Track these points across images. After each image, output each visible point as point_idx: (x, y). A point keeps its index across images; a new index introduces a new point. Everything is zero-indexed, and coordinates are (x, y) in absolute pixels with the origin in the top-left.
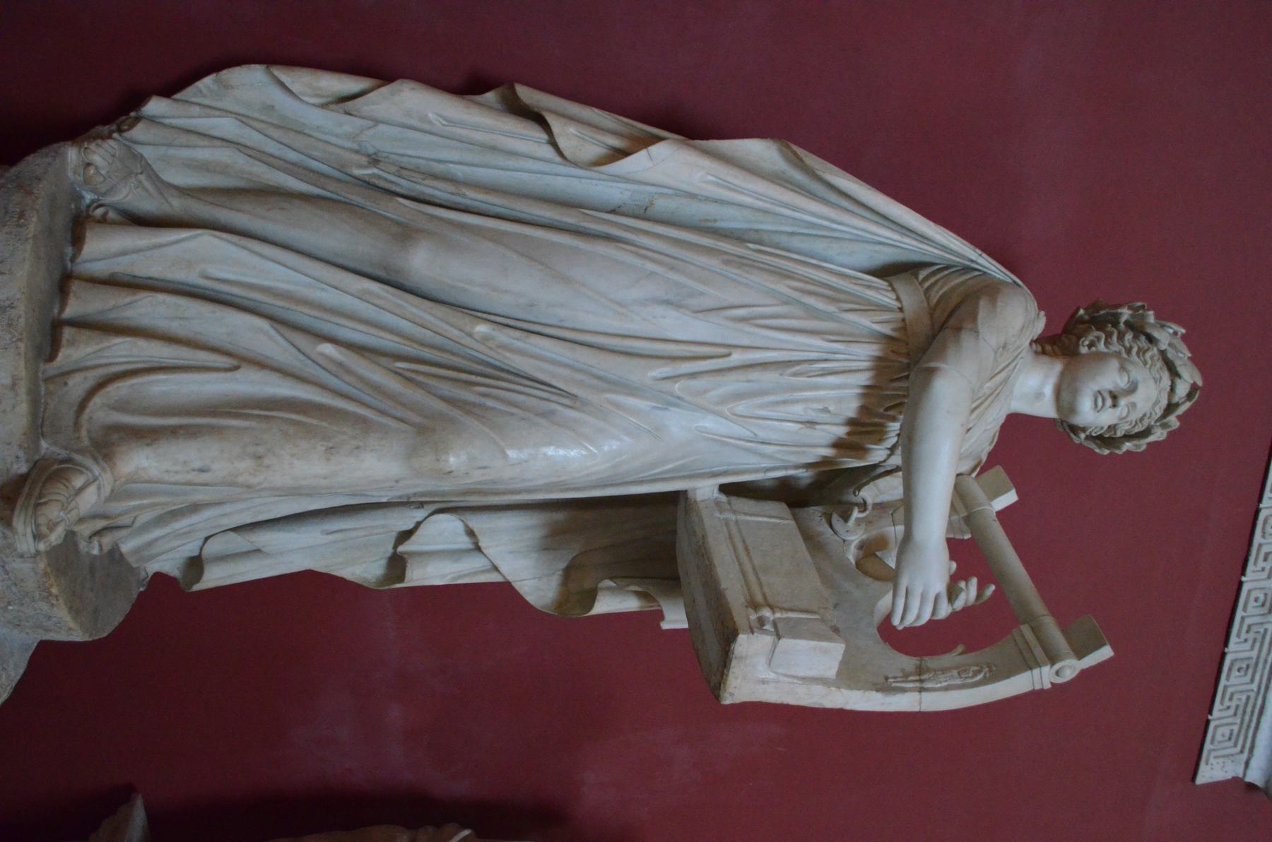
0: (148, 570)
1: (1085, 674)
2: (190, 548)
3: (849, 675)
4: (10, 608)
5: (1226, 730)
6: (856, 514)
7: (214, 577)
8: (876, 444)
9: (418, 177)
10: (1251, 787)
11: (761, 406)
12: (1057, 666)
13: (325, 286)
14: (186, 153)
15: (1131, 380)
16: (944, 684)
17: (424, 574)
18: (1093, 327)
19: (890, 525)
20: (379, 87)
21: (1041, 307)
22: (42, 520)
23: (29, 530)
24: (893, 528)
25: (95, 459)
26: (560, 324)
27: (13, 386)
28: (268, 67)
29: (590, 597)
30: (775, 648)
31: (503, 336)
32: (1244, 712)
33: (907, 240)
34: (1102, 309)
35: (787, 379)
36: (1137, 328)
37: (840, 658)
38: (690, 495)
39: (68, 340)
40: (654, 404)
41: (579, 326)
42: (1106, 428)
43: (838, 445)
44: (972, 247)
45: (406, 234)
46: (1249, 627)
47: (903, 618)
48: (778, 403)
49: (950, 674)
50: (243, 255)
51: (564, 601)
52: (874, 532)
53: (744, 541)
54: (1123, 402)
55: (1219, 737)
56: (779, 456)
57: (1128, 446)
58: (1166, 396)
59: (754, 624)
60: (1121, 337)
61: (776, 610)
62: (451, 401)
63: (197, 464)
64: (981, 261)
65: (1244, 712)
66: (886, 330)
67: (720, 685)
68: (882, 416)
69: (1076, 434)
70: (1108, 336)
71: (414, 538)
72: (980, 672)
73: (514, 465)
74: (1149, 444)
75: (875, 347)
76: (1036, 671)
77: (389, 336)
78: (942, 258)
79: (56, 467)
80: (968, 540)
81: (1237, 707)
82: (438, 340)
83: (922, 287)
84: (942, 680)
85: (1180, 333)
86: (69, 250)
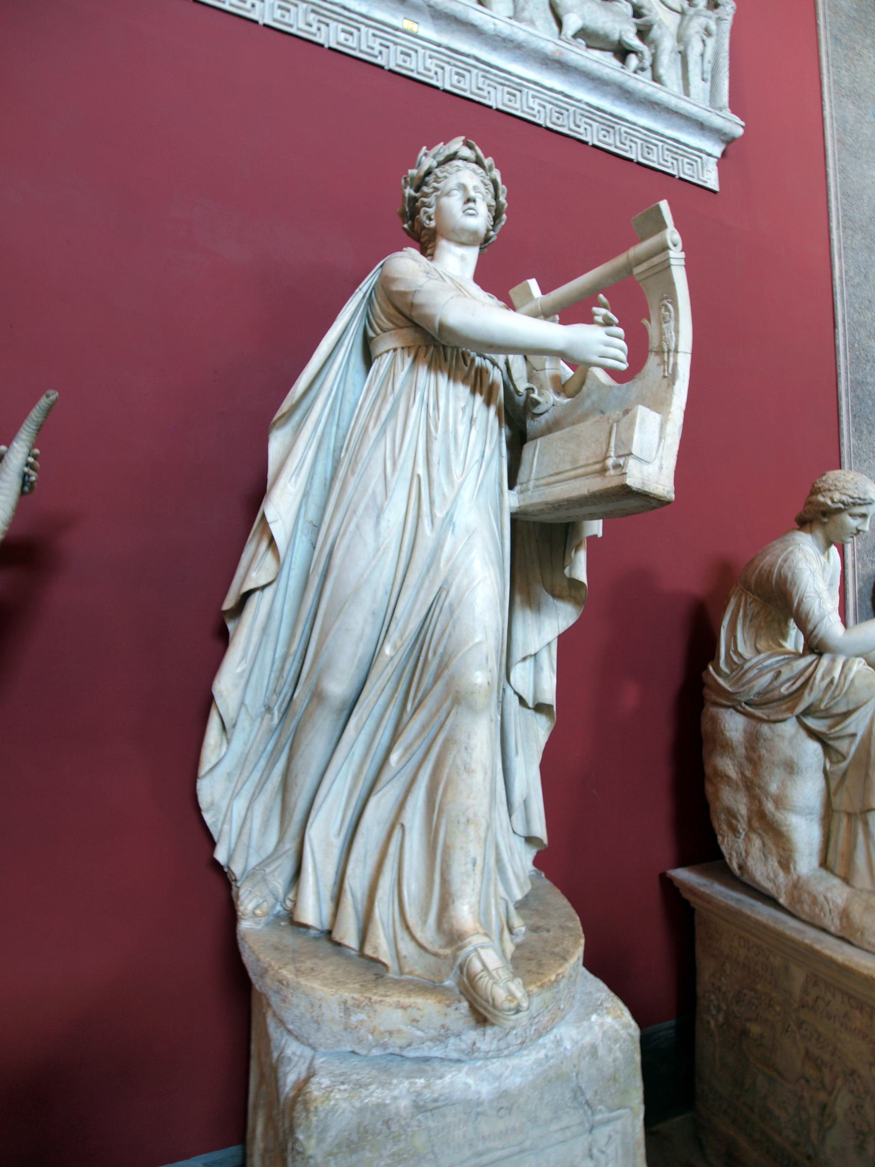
0: (531, 870)
1: (677, 226)
2: (519, 844)
3: (660, 405)
4: (562, 1007)
5: (687, 166)
6: (535, 396)
7: (540, 830)
8: (490, 375)
9: (282, 682)
10: (724, 154)
11: (457, 455)
12: (671, 245)
13: (351, 753)
14: (255, 834)
15: (457, 188)
16: (673, 333)
17: (549, 694)
18: (418, 216)
19: (545, 372)
20: (216, 704)
21: (401, 250)
22: (507, 1005)
23: (514, 1017)
24: (547, 371)
25: (461, 948)
26: (389, 594)
27: (404, 1008)
28: (199, 778)
29: (575, 584)
30: (638, 458)
31: (394, 634)
32: (676, 153)
33: (346, 342)
34: (405, 209)
35: (439, 435)
36: (420, 184)
37: (648, 410)
38: (514, 511)
39: (374, 952)
40: (450, 532)
41: (391, 581)
42: (489, 213)
43: (488, 403)
44: (354, 295)
45: (318, 696)
46: (622, 143)
47: (621, 361)
48: (456, 443)
49: (665, 330)
50: (326, 807)
51: (576, 602)
52: (548, 383)
53: (551, 475)
54: (472, 194)
55: (690, 173)
56: (493, 446)
57: (502, 199)
58: (470, 164)
59: (618, 472)
60: (426, 195)
61: (608, 455)
62: (437, 678)
63: (470, 866)
64: (364, 290)
65: (676, 153)
66: (409, 361)
67: (661, 500)
68: (470, 369)
69: (490, 238)
70: (424, 205)
71: (524, 697)
72: (666, 307)
73: (486, 637)
74: (503, 183)
75: (420, 369)
76: (672, 262)
77: (388, 713)
78: (362, 317)
79: (465, 979)
80: (560, 317)
81: (673, 158)
82: (394, 679)
83: (380, 334)
84: (670, 336)
85: (427, 151)
86: (312, 932)
